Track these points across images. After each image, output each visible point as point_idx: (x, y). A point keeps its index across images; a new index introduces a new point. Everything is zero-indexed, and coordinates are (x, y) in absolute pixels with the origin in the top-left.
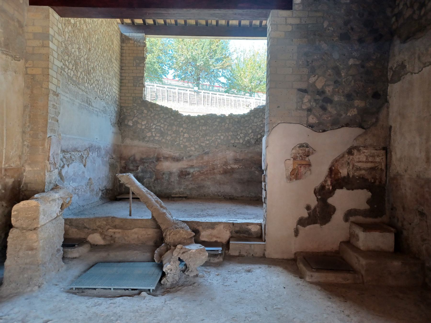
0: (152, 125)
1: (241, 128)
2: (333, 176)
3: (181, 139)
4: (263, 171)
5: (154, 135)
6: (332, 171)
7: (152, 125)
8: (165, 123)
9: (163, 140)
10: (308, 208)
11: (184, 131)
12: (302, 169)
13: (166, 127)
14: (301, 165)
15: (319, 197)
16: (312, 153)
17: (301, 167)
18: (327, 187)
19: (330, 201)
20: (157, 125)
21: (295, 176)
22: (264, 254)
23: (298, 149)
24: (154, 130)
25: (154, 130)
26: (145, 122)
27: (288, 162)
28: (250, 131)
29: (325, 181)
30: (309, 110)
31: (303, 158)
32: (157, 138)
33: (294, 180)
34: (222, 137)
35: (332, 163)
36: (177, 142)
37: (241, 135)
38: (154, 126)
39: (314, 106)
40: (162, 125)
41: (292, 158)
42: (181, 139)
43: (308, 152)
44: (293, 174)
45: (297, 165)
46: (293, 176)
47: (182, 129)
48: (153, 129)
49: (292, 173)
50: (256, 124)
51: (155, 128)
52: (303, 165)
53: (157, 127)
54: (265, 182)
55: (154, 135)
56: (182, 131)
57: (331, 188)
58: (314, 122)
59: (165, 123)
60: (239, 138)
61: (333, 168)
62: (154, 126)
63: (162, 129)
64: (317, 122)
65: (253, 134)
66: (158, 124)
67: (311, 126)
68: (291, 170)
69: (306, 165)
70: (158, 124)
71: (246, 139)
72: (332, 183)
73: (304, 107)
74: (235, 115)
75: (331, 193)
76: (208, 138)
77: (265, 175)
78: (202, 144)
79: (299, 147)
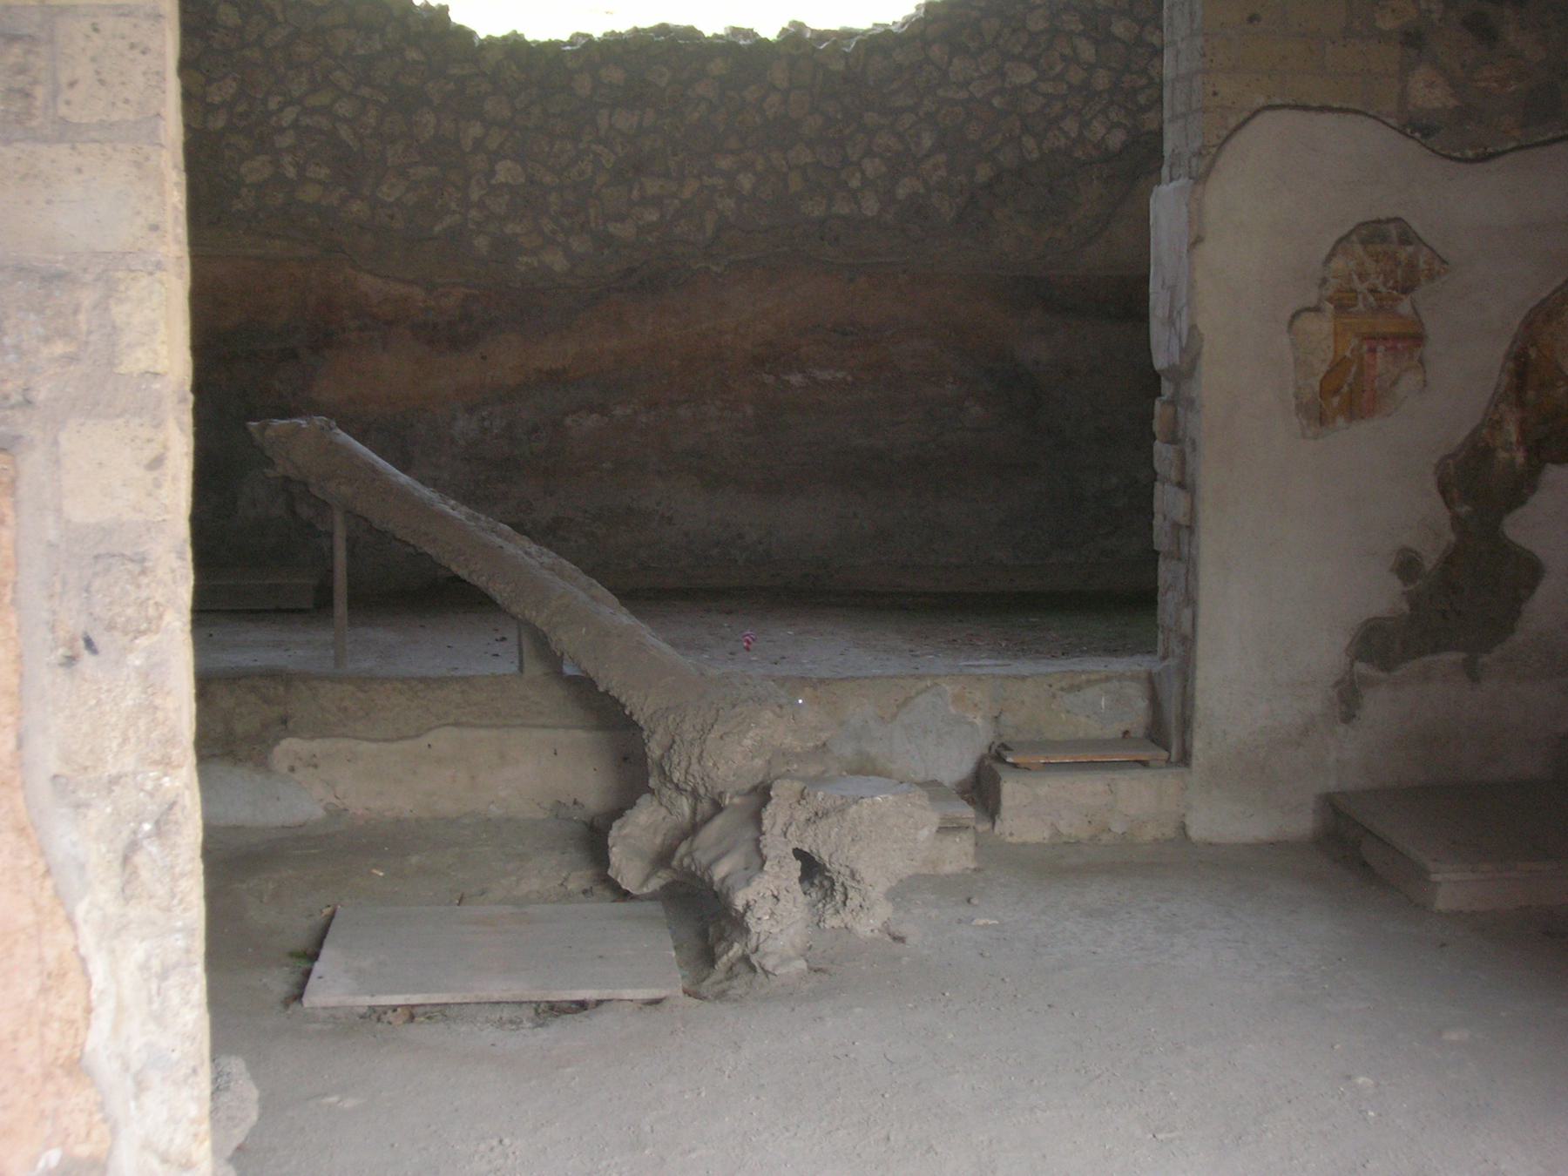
0: (273, 105)
1: (871, 118)
2: (1531, 395)
3: (475, 196)
4: (1157, 377)
5: (291, 172)
6: (1524, 370)
7: (273, 105)
8: (365, 91)
9: (356, 207)
10: (1407, 566)
11: (492, 144)
12: (1381, 362)
13: (371, 118)
14: (1371, 338)
15: (1464, 509)
16: (1431, 277)
17: (1373, 351)
18: (1502, 455)
19: (1526, 527)
20: (312, 101)
21: (1341, 396)
22: (1183, 828)
23: (1358, 249)
24: (287, 140)
25: (287, 140)
26: (230, 87)
27: (1309, 323)
28: (927, 141)
29: (1495, 424)
30: (1412, 39)
31: (1376, 296)
32: (310, 194)
33: (1341, 421)
34: (746, 182)
35: (1528, 324)
36: (448, 221)
37: (872, 167)
38: (289, 115)
39: (1435, 16)
40: (344, 108)
41: (1330, 300)
42: (475, 196)
43: (1412, 266)
44: (1336, 391)
45: (1355, 342)
46: (1336, 400)
47: (476, 130)
48: (281, 130)
49: (1329, 387)
50: (963, 95)
51: (295, 125)
52: (1385, 339)
53: (305, 121)
54: (1173, 440)
55: (291, 172)
56: (478, 144)
57: (1520, 457)
58: (1437, 104)
59: (365, 91)
60: (855, 183)
61: (1533, 353)
62: (289, 115)
63: (344, 132)
64: (1452, 103)
65: (941, 158)
66: (323, 99)
67: (1419, 128)
68: (1325, 368)
69: (1397, 337)
70: (323, 99)
71: (901, 193)
72: (1523, 432)
73: (1387, 23)
74: (822, 36)
75: (1520, 489)
76: (653, 187)
77: (1172, 402)
78: (614, 228)
79: (1364, 242)
